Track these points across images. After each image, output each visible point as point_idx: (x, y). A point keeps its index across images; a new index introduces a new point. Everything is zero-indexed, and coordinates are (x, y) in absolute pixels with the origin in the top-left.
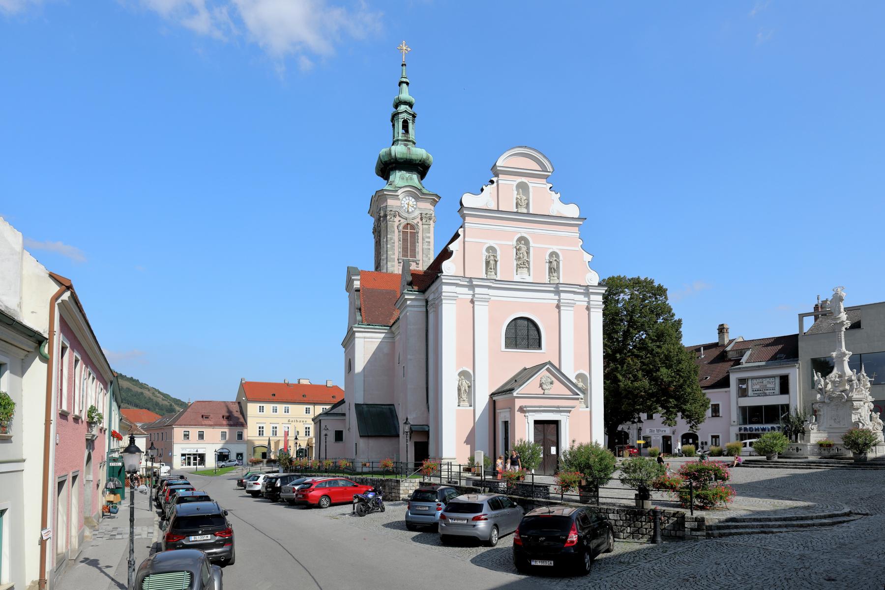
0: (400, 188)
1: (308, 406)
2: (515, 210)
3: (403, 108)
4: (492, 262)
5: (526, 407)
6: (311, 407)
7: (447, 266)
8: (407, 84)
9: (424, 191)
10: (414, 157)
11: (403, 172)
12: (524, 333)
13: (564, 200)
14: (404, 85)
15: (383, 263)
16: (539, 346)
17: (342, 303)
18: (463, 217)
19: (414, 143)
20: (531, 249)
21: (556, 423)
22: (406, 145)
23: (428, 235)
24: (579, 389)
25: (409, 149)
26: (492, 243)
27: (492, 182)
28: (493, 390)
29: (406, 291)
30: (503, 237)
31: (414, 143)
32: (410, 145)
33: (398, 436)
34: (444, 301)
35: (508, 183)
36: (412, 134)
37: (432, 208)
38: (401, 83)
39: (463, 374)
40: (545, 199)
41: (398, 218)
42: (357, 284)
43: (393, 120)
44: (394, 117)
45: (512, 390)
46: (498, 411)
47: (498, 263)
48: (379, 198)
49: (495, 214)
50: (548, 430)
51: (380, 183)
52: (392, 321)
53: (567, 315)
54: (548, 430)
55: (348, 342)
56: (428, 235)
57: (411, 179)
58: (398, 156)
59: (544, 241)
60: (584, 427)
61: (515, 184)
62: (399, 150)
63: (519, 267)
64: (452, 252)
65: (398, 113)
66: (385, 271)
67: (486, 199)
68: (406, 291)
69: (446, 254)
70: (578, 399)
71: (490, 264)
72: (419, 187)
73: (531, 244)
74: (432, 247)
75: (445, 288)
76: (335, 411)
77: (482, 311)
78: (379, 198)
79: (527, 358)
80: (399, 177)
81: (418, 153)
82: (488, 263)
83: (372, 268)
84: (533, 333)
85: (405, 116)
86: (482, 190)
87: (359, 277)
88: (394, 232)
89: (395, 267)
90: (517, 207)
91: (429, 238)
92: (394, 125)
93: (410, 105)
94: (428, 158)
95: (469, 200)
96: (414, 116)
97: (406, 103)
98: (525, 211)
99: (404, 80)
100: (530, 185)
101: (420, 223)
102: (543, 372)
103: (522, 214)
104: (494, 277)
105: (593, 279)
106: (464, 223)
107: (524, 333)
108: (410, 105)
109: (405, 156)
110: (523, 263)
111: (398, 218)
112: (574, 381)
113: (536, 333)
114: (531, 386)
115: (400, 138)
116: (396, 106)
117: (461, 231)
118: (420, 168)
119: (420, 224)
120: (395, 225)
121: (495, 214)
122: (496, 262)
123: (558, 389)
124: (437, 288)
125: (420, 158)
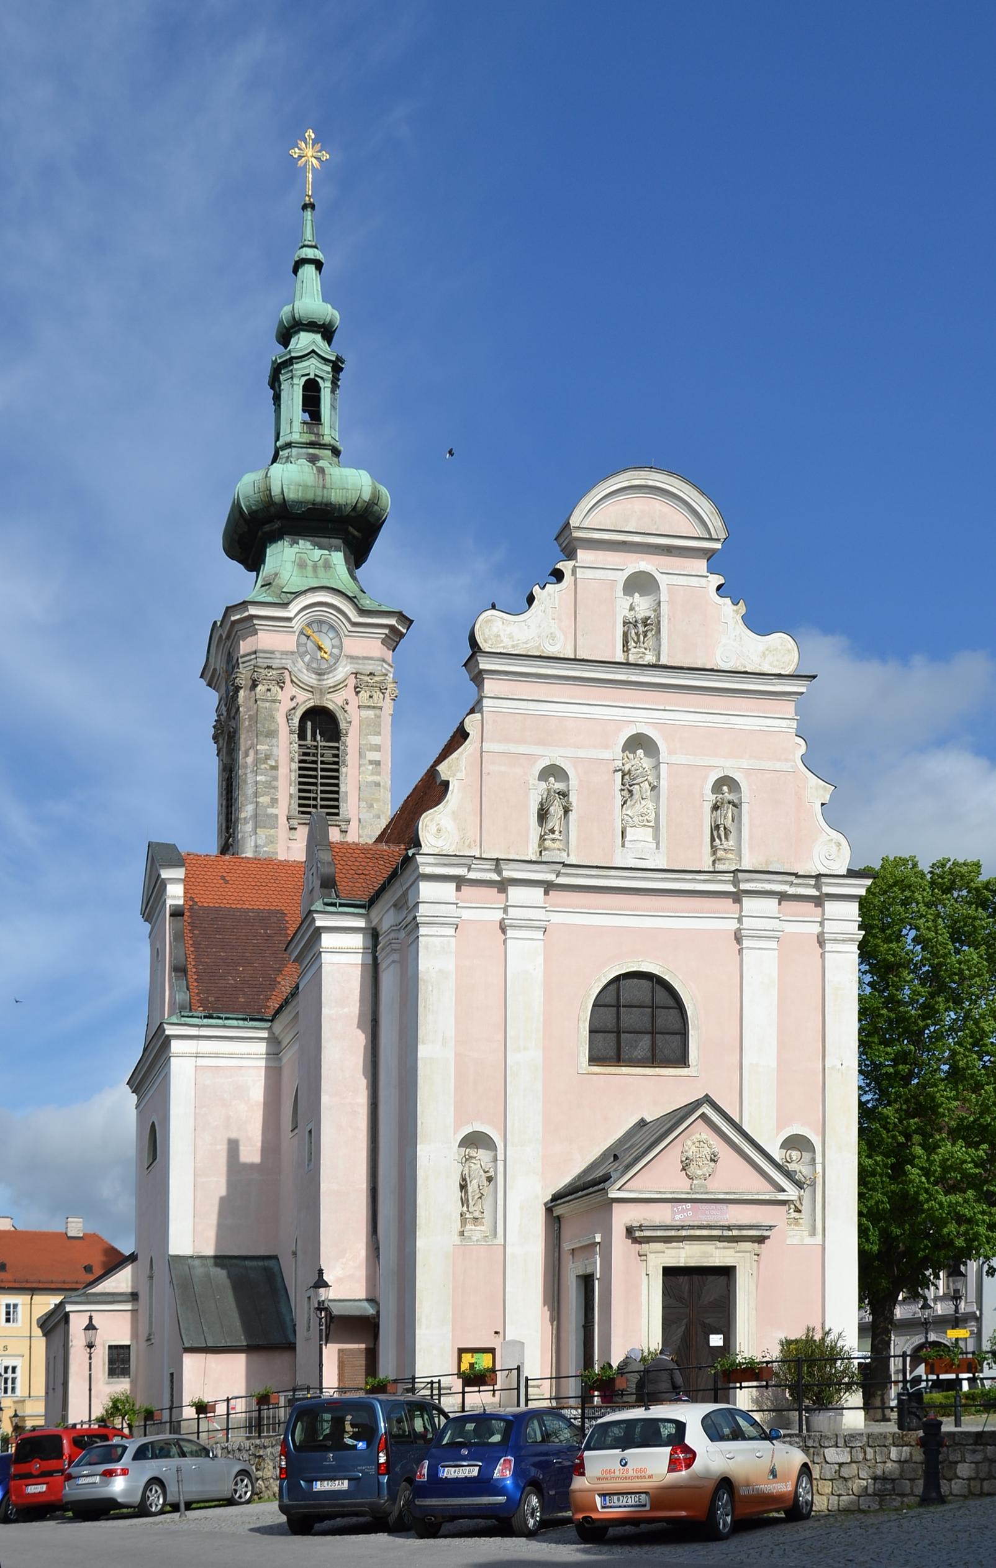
0: (298, 594)
1: (12, 1299)
2: (620, 657)
3: (304, 341)
5: (641, 1228)
6: (21, 1300)
7: (438, 830)
8: (318, 265)
9: (367, 603)
10: (336, 497)
11: (304, 545)
12: (640, 1021)
13: (759, 622)
14: (309, 270)
15: (245, 829)
17: (131, 962)
18: (478, 678)
19: (336, 452)
20: (663, 768)
21: (727, 1273)
22: (313, 459)
23: (375, 740)
24: (788, 1175)
25: (321, 470)
28: (564, 1180)
29: (318, 905)
30: (587, 729)
31: (336, 452)
32: (326, 459)
33: (291, 1347)
34: (422, 931)
35: (596, 574)
36: (329, 431)
37: (389, 655)
39: (475, 1141)
40: (710, 625)
41: (290, 689)
42: (175, 894)
43: (275, 382)
44: (278, 371)
45: (606, 1178)
47: (572, 816)
48: (230, 630)
50: (699, 1297)
51: (234, 581)
52: (274, 1005)
53: (762, 962)
54: (699, 1297)
55: (150, 1074)
56: (375, 740)
57: (327, 566)
58: (291, 495)
59: (701, 740)
60: (805, 1284)
61: (622, 577)
62: (291, 478)
64: (446, 784)
65: (291, 361)
66: (249, 854)
68: (318, 905)
69: (430, 791)
70: (784, 1203)
72: (350, 587)
73: (664, 756)
74: (385, 779)
75: (426, 890)
78: (230, 630)
79: (648, 1092)
80: (285, 558)
81: (351, 483)
83: (210, 845)
85: (312, 367)
86: (531, 599)
87: (179, 873)
88: (272, 734)
89: (279, 837)
90: (626, 649)
91: (377, 748)
92: (277, 398)
93: (327, 332)
94: (375, 500)
95: (498, 630)
96: (337, 367)
97: (312, 326)
98: (650, 658)
99: (310, 253)
101: (354, 701)
102: (697, 1138)
103: (638, 661)
104: (563, 857)
105: (830, 853)
106: (479, 701)
107: (640, 1021)
108: (327, 332)
109: (310, 496)
111: (290, 689)
112: (777, 1154)
113: (678, 1018)
114: (659, 1174)
115: (296, 437)
116: (285, 336)
117: (472, 724)
118: (353, 530)
119: (352, 709)
120: (283, 706)
123: (733, 1175)
124: (405, 894)
125: (351, 497)
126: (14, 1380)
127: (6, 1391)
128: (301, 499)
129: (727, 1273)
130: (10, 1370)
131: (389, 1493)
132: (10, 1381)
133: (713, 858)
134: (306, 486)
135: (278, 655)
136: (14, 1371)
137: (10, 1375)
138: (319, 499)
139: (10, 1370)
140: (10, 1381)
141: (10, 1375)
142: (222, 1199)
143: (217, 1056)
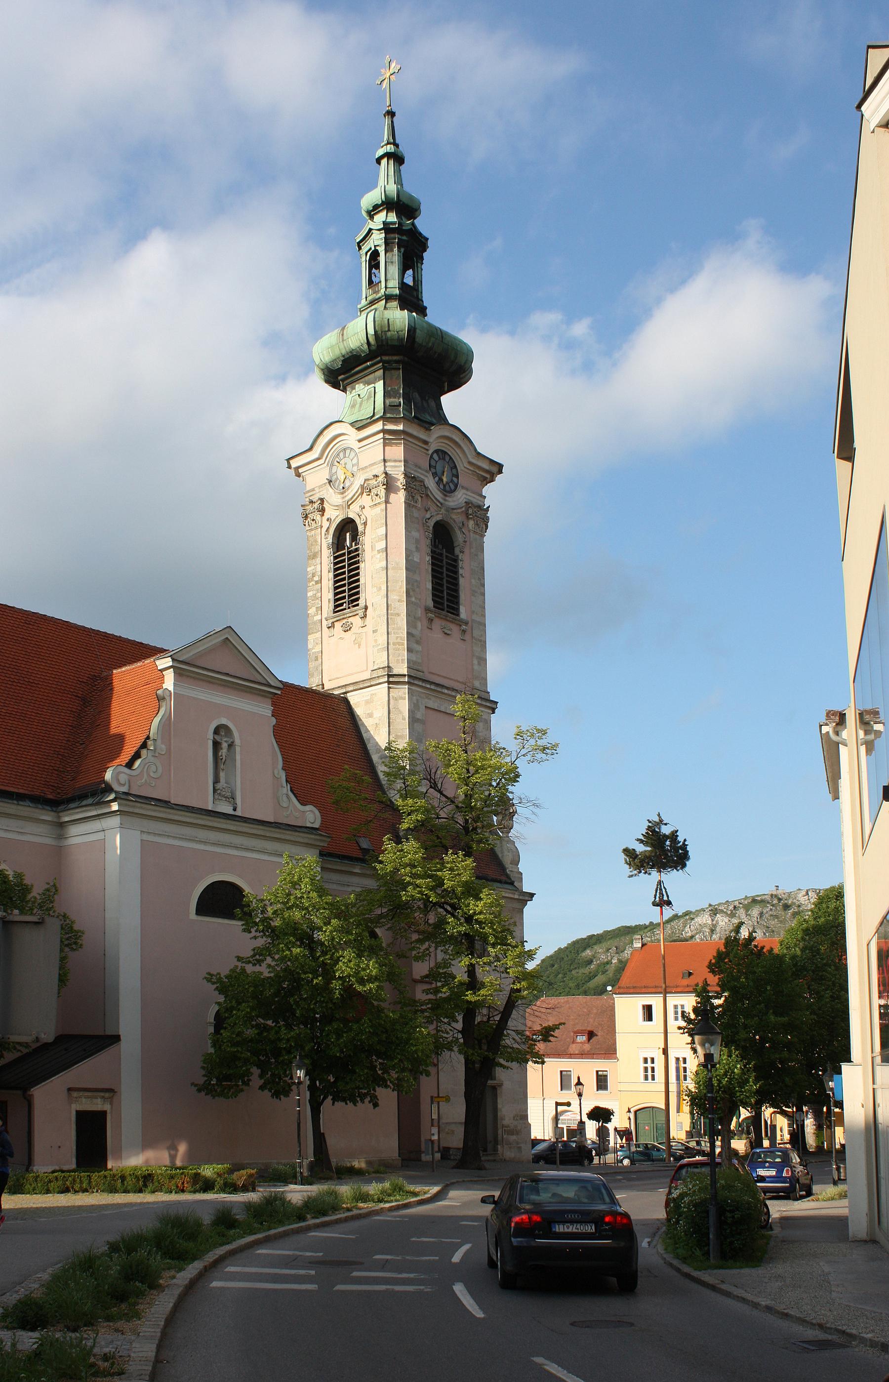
21: (104, 1114)
109: (337, 353)
126: (653, 1069)
127: (646, 1078)
128: (334, 358)
129: (104, 1114)
130: (649, 1060)
131: (420, 1285)
132: (650, 1070)
133: (292, 471)
134: (332, 347)
135: (317, 490)
136: (653, 1062)
137: (649, 1065)
138: (344, 352)
139: (649, 1060)
140: (650, 1070)
141: (649, 1065)
142: (560, 949)
143: (247, 849)
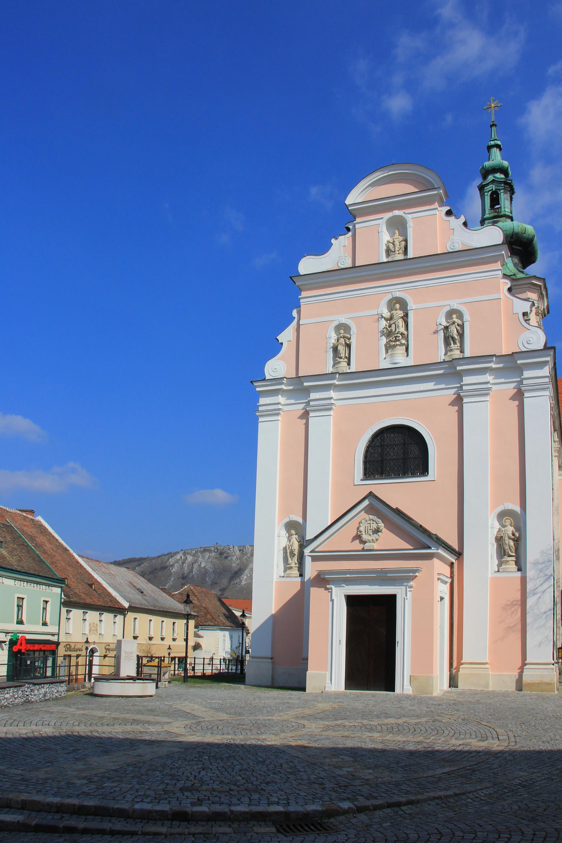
4: (341, 348)
8: (498, 146)
16: (424, 470)
21: (392, 599)
26: (343, 319)
27: (348, 230)
38: (489, 148)
46: (519, 626)
49: (355, 273)
59: (429, 300)
63: (389, 347)
67: (338, 253)
71: (341, 349)
73: (411, 305)
76: (149, 664)
77: (323, 427)
82: (335, 349)
84: (415, 450)
100: (409, 218)
103: (402, 264)
110: (394, 338)
121: (355, 273)
122: (349, 346)
